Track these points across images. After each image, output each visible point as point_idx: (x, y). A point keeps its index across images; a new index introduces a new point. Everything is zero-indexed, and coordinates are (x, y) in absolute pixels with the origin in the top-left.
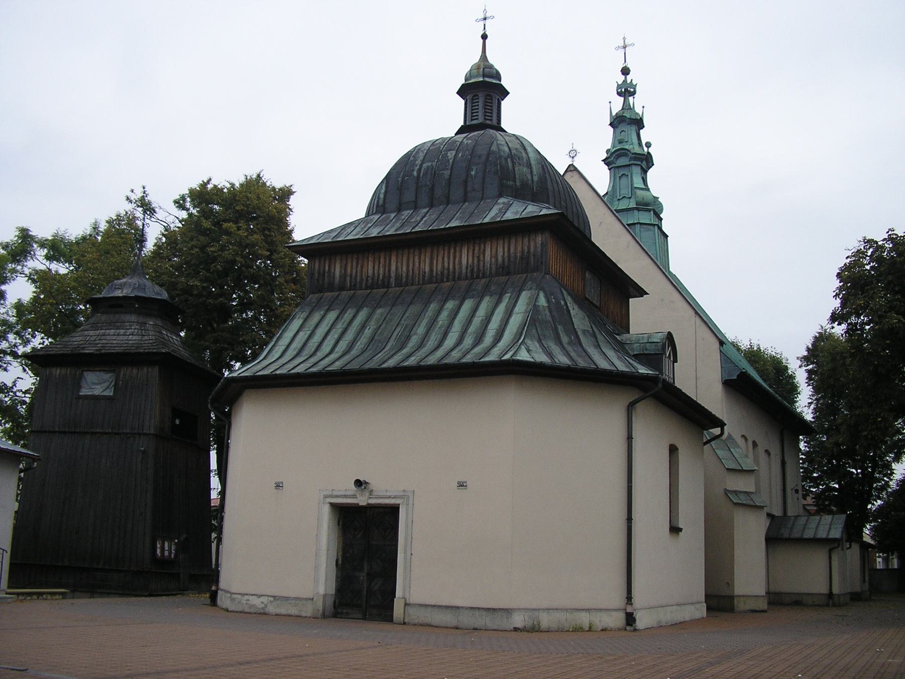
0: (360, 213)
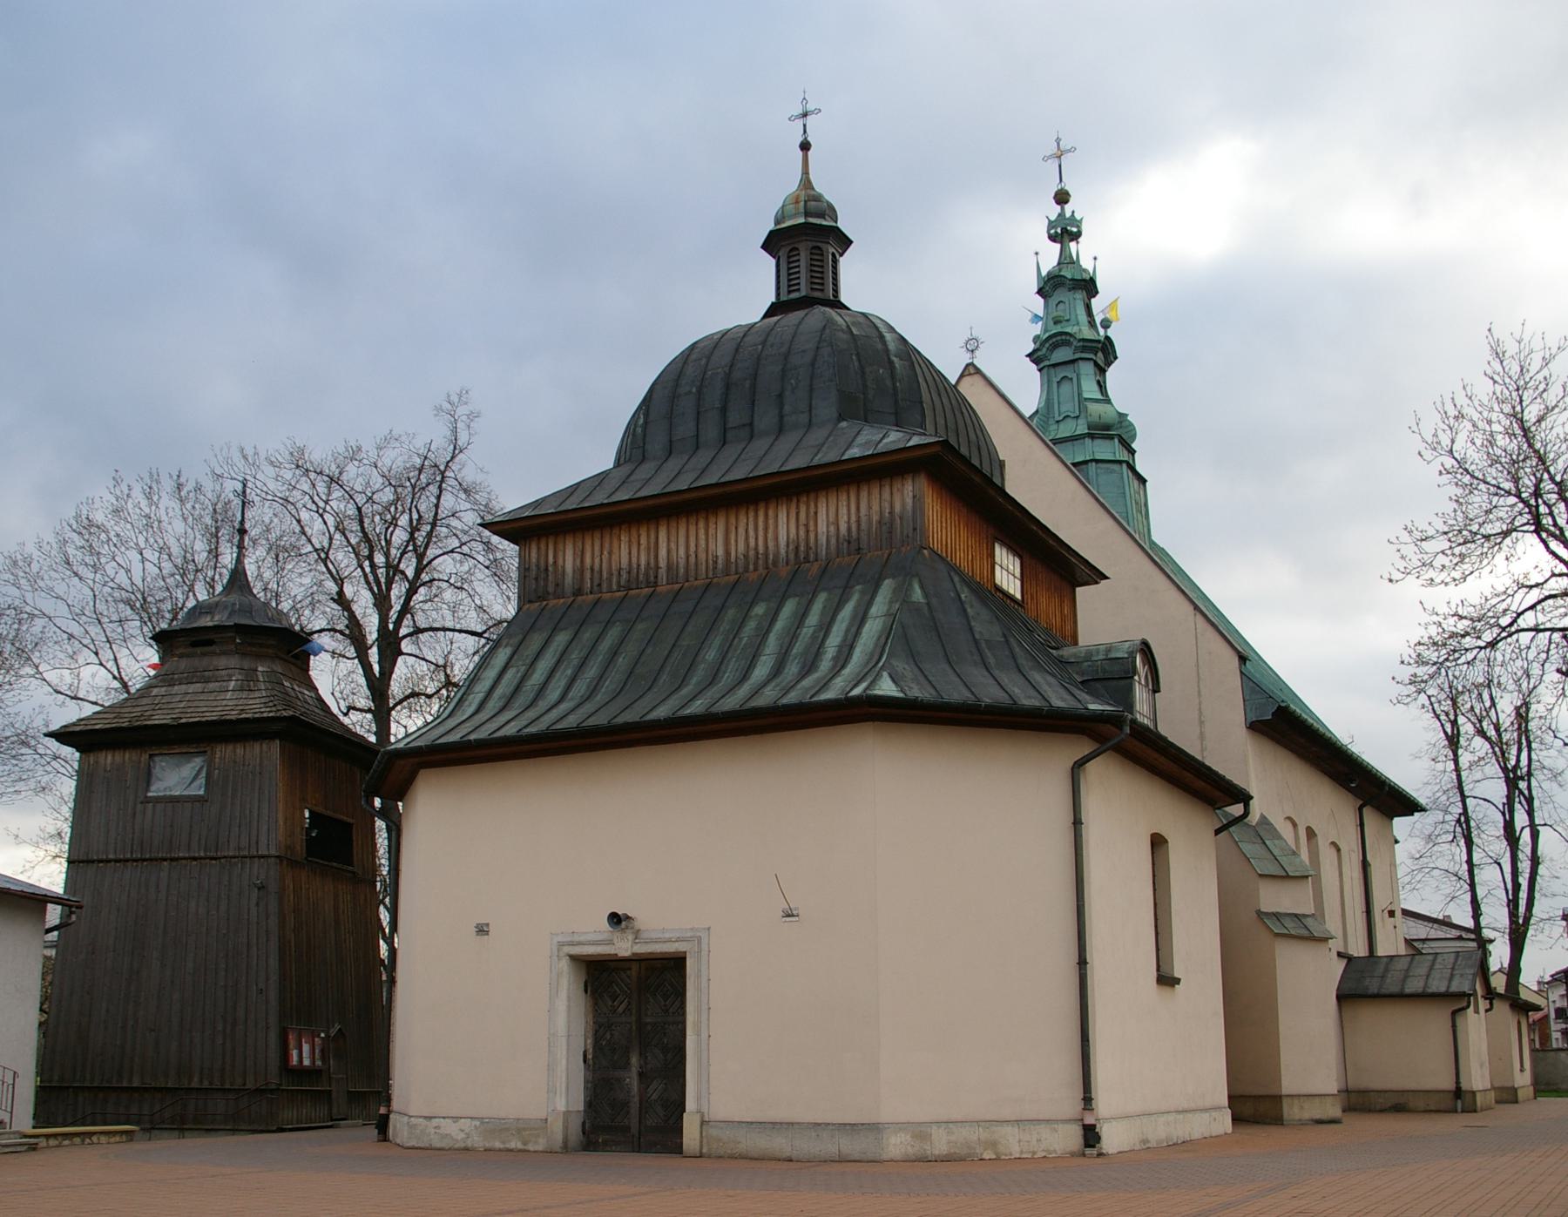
0: (602, 459)
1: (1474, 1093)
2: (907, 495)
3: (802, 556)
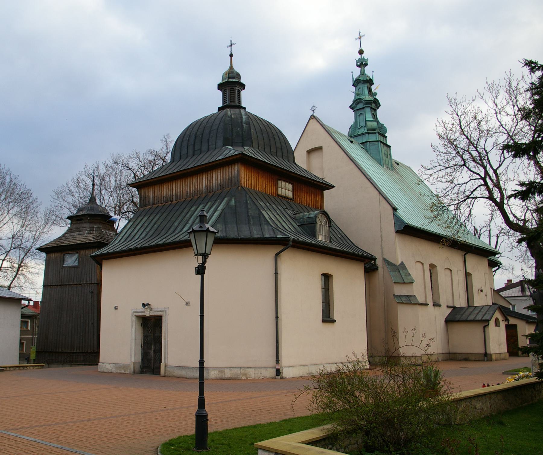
1: (491, 354)
2: (236, 169)
3: (209, 190)
